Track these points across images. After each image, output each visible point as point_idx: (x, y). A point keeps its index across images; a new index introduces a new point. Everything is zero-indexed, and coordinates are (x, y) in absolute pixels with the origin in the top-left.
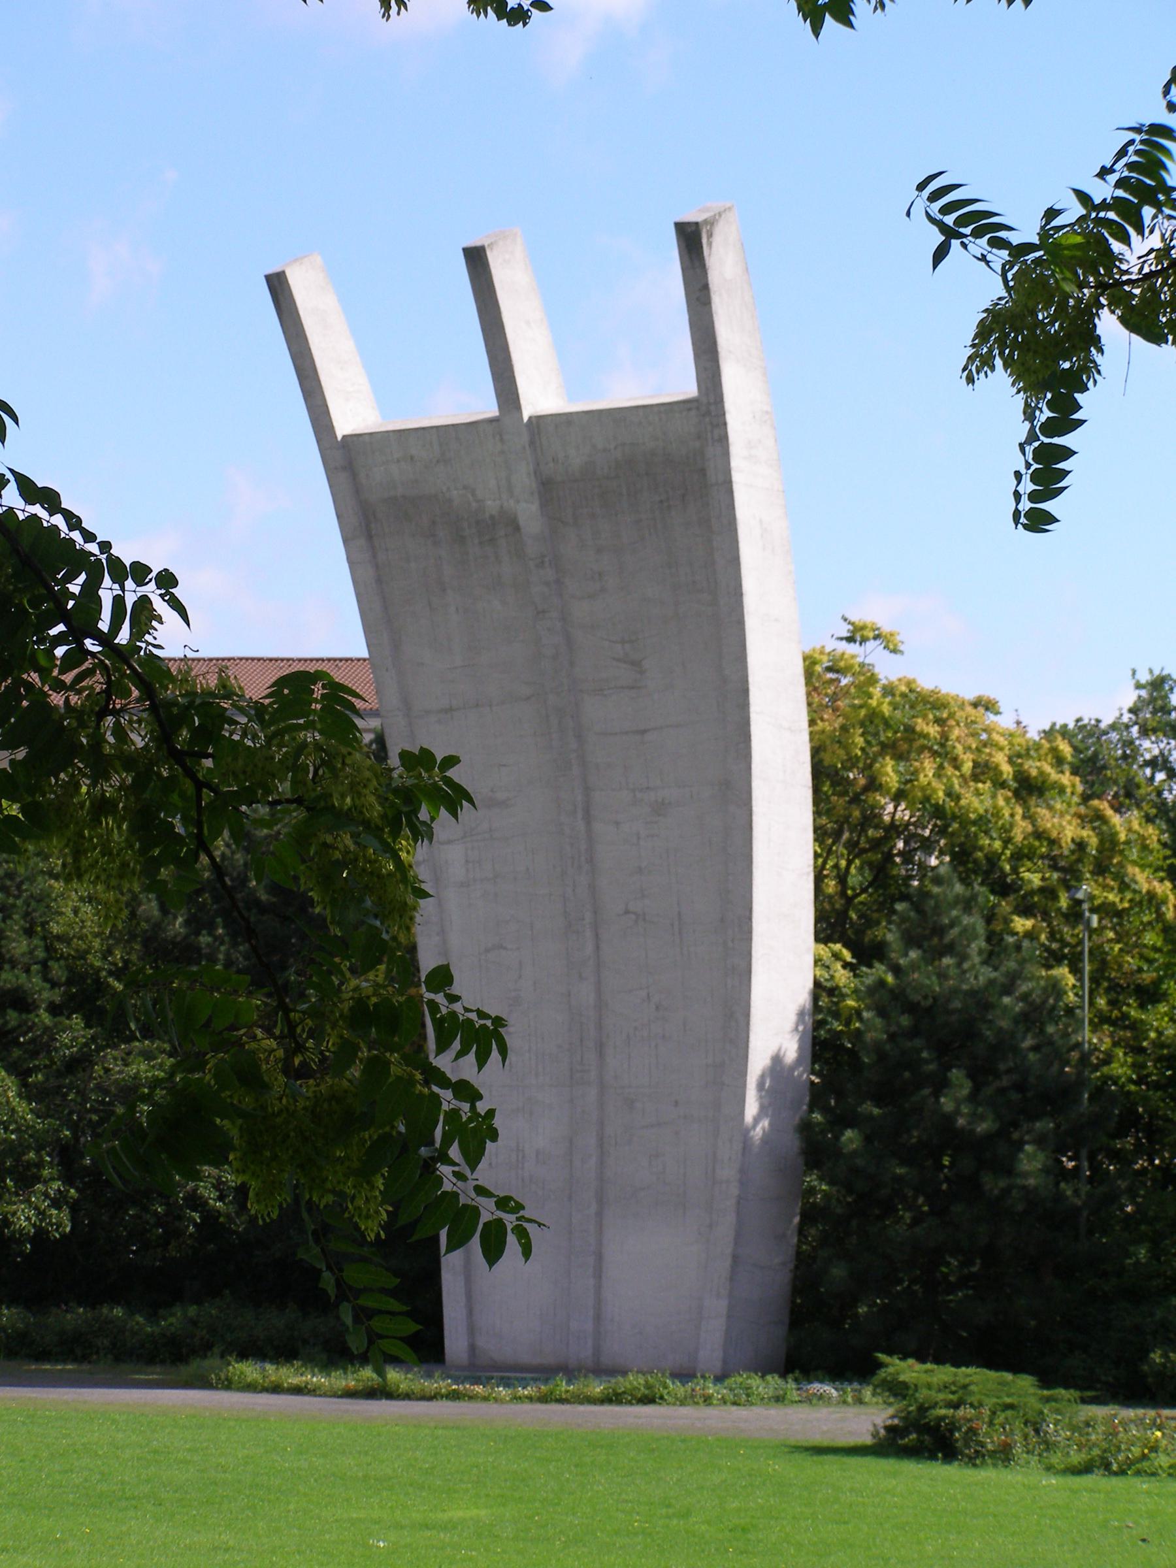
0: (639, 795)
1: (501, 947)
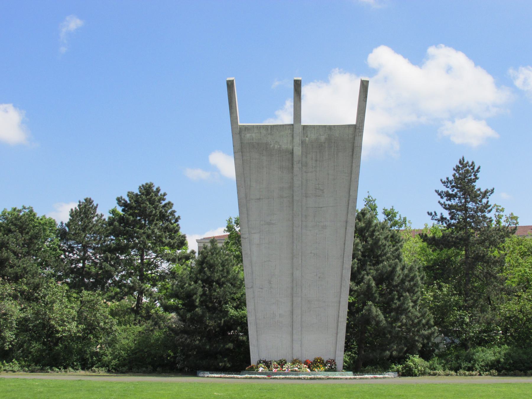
0: (318, 223)
1: (269, 261)
